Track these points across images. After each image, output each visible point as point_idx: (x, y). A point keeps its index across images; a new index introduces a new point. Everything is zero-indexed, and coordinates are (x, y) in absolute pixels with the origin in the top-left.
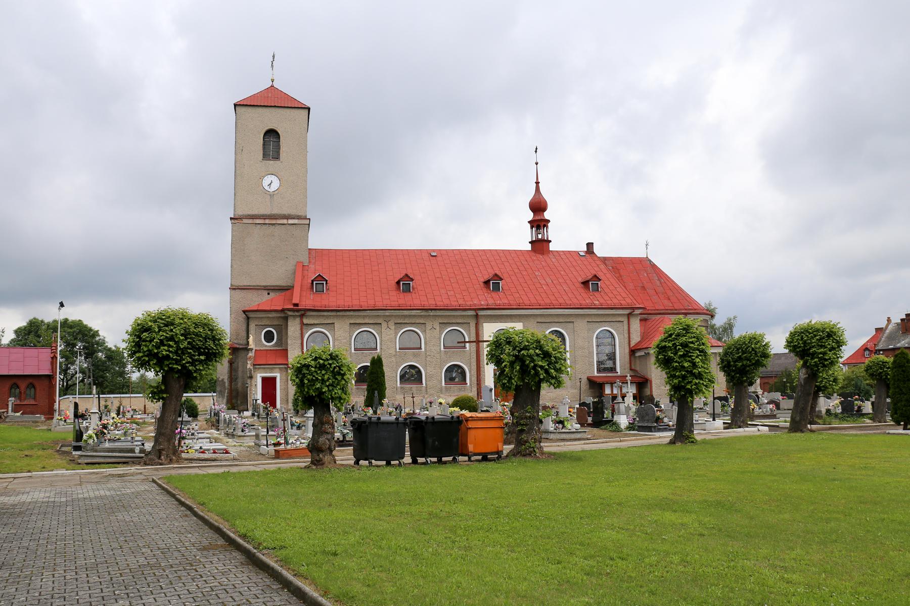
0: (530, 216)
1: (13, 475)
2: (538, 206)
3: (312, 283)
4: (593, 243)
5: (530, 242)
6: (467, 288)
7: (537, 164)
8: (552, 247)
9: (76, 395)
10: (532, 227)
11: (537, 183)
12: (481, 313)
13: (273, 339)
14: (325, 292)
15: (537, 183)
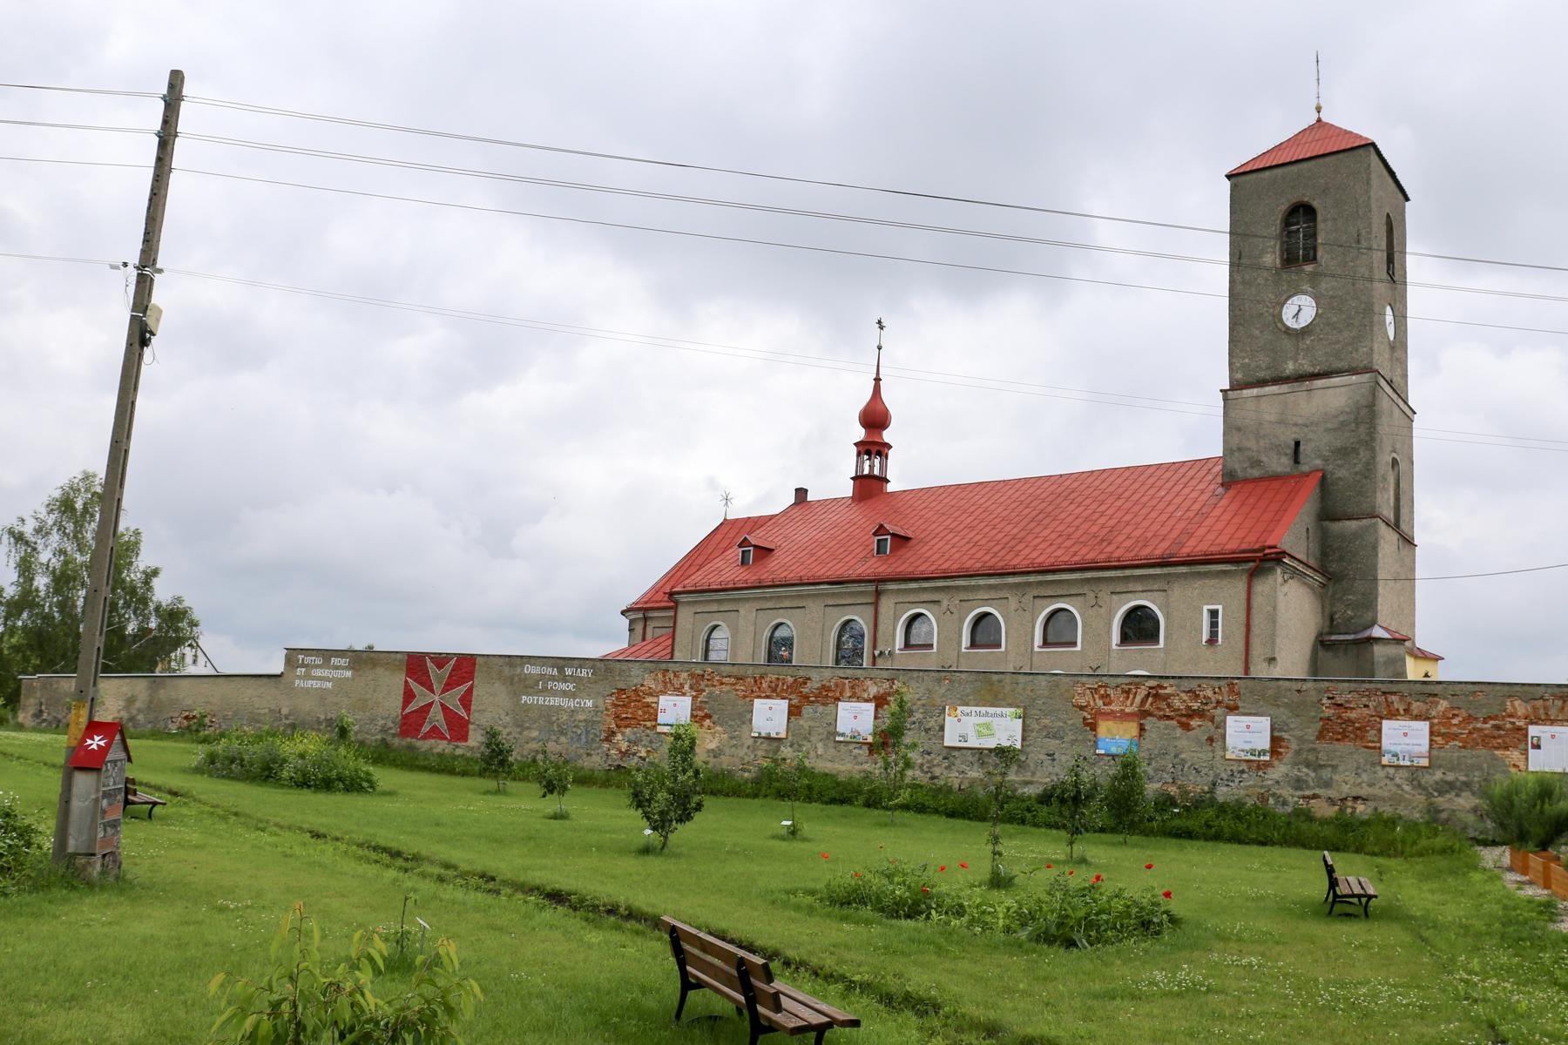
0: (860, 433)
2: (875, 418)
5: (852, 478)
7: (880, 348)
8: (890, 488)
9: (104, 658)
11: (877, 380)
15: (877, 380)
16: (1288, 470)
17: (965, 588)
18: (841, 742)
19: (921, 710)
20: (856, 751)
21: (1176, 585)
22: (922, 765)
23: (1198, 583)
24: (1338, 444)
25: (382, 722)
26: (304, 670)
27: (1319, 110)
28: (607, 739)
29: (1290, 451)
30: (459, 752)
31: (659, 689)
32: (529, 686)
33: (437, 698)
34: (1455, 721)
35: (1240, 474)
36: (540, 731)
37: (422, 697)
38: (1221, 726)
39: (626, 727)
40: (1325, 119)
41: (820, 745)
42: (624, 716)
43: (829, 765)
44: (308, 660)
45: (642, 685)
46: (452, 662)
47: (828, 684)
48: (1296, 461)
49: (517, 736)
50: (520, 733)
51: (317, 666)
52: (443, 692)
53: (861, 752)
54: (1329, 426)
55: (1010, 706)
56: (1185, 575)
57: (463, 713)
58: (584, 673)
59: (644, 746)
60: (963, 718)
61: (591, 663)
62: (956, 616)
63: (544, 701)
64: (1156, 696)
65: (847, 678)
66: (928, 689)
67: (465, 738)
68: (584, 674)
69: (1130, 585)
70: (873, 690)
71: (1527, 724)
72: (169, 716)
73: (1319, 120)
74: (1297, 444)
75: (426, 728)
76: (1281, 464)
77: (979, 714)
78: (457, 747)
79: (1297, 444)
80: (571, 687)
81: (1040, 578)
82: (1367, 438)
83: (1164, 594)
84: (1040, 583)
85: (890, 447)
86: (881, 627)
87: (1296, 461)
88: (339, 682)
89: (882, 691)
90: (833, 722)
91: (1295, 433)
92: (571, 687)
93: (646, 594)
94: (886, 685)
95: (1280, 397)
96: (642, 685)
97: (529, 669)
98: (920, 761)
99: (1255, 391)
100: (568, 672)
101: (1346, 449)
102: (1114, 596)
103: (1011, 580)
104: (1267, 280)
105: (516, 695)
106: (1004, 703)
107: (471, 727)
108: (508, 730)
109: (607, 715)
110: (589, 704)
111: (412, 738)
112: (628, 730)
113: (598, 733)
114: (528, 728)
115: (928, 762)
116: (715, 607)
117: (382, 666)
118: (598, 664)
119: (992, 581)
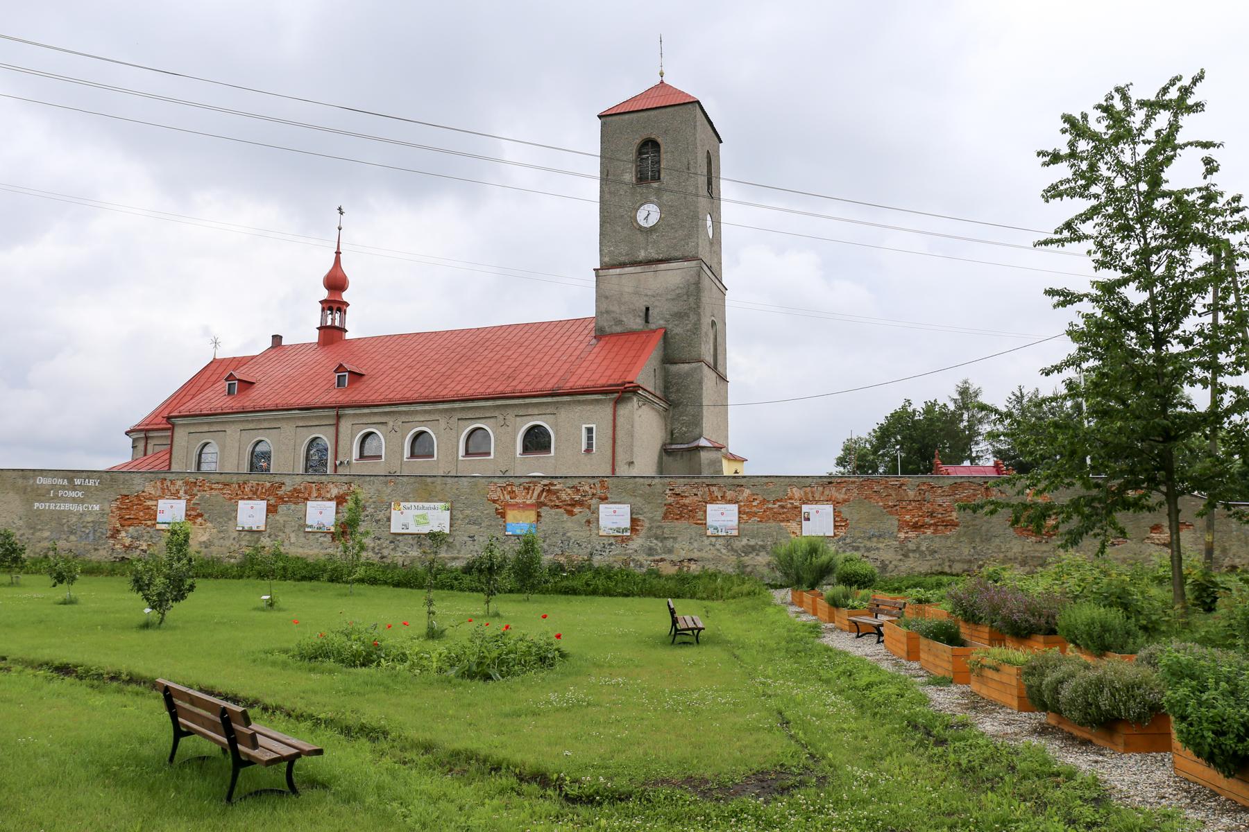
1: (190, 692)
2: (336, 283)
4: (281, 337)
7: (340, 229)
8: (348, 336)
10: (323, 310)
11: (338, 253)
12: (151, 434)
13: (546, 430)
15: (338, 253)
16: (641, 327)
17: (406, 413)
19: (372, 506)
20: (322, 539)
22: (374, 547)
24: (676, 309)
28: (113, 536)
29: (643, 314)
34: (754, 504)
36: (52, 533)
38: (596, 511)
39: (129, 526)
41: (293, 535)
42: (128, 517)
43: (300, 550)
45: (143, 492)
48: (647, 321)
49: (30, 536)
53: (325, 539)
54: (669, 297)
55: (441, 501)
56: (569, 403)
59: (145, 541)
60: (405, 511)
61: (98, 474)
62: (399, 434)
63: (56, 506)
65: (314, 483)
66: (378, 490)
70: (335, 492)
73: (662, 82)
74: (647, 309)
76: (636, 323)
79: (647, 309)
80: (80, 494)
81: (463, 405)
82: (695, 306)
83: (554, 416)
84: (463, 409)
85: (347, 305)
86: (340, 443)
87: (647, 321)
89: (341, 492)
90: (303, 517)
92: (80, 494)
96: (143, 492)
97: (41, 481)
98: (372, 545)
99: (618, 271)
100: (77, 482)
101: (681, 313)
102: (518, 419)
103: (441, 406)
108: (21, 532)
109: (113, 517)
110: (97, 508)
112: (131, 529)
114: (40, 530)
116: (206, 428)
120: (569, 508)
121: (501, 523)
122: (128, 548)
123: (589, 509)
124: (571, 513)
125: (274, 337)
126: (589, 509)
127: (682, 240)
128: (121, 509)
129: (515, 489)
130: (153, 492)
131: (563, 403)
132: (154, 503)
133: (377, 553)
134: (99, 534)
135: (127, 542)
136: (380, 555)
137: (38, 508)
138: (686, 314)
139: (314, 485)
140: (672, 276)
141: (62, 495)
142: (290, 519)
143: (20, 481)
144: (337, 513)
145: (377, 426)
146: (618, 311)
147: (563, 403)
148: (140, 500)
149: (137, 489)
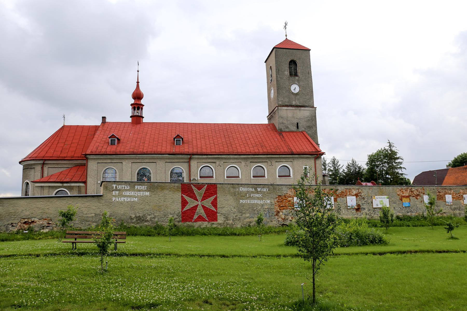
2: (138, 96)
3: (174, 140)
6: (222, 142)
7: (138, 71)
8: (144, 120)
11: (138, 82)
14: (181, 145)
15: (138, 82)
16: (296, 130)
17: (225, 158)
18: (349, 209)
19: (367, 198)
20: (353, 211)
21: (295, 160)
22: (369, 214)
23: (301, 160)
24: (308, 125)
25: (171, 216)
26: (117, 192)
27: (286, 36)
28: (277, 215)
29: (296, 125)
30: (214, 226)
31: (293, 195)
32: (243, 196)
33: (199, 203)
34: (454, 195)
35: (283, 130)
36: (250, 214)
37: (191, 203)
38: (423, 198)
39: (283, 209)
40: (289, 38)
41: (343, 210)
42: (282, 205)
43: (346, 216)
44: (120, 187)
45: (287, 194)
46: (206, 187)
47: (343, 191)
48: (298, 128)
49: (240, 217)
50: (241, 215)
51: (127, 190)
52: (202, 200)
53: (354, 211)
54: (306, 120)
55: (385, 195)
56: (297, 158)
57: (213, 209)
58: (265, 190)
59: (291, 216)
60: (377, 199)
61: (267, 186)
62: (222, 167)
63: (250, 202)
64: (411, 191)
65: (347, 189)
66: (367, 192)
67: (216, 219)
68: (265, 190)
69: (282, 160)
70: (355, 192)
71: (463, 194)
72: (10, 222)
73: (286, 39)
74: (298, 124)
75: (196, 217)
76: (294, 129)
77: (380, 198)
78: (213, 224)
79: (298, 124)
80: (260, 195)
81: (252, 156)
82: (315, 124)
83: (291, 163)
84: (252, 158)
85: (143, 105)
86: (192, 170)
87: (298, 128)
88: (143, 199)
89: (357, 193)
90: (346, 203)
91: (297, 121)
92: (260, 195)
93: (30, 154)
94: (357, 191)
95: (293, 111)
96: (287, 194)
97: (242, 189)
98: (368, 213)
99: (286, 108)
100: (259, 190)
101: (310, 126)
102: (276, 163)
103: (242, 156)
104: (286, 78)
105: (237, 200)
106: (384, 195)
107: (218, 214)
108: (236, 215)
109: (276, 206)
110: (269, 202)
111: (189, 222)
112: (284, 211)
113: (273, 213)
114: (244, 213)
115: (370, 213)
116: (109, 161)
117: (168, 190)
118: (270, 186)
119: (236, 156)
120: (416, 197)
121: (401, 203)
122: (284, 219)
123: (421, 197)
124: (417, 198)
125: (103, 117)
126: (421, 197)
127: (308, 100)
128: (278, 202)
129: (403, 190)
130: (291, 194)
131: (296, 158)
132: (291, 199)
133: (370, 216)
134: (271, 214)
135: (283, 217)
136: (371, 216)
137: (242, 202)
138: (312, 127)
139: (348, 190)
140: (304, 113)
141: (252, 196)
142: (342, 204)
143: (232, 189)
144: (356, 201)
145: (210, 163)
146: (287, 123)
147: (296, 158)
148: (286, 198)
149: (285, 192)
